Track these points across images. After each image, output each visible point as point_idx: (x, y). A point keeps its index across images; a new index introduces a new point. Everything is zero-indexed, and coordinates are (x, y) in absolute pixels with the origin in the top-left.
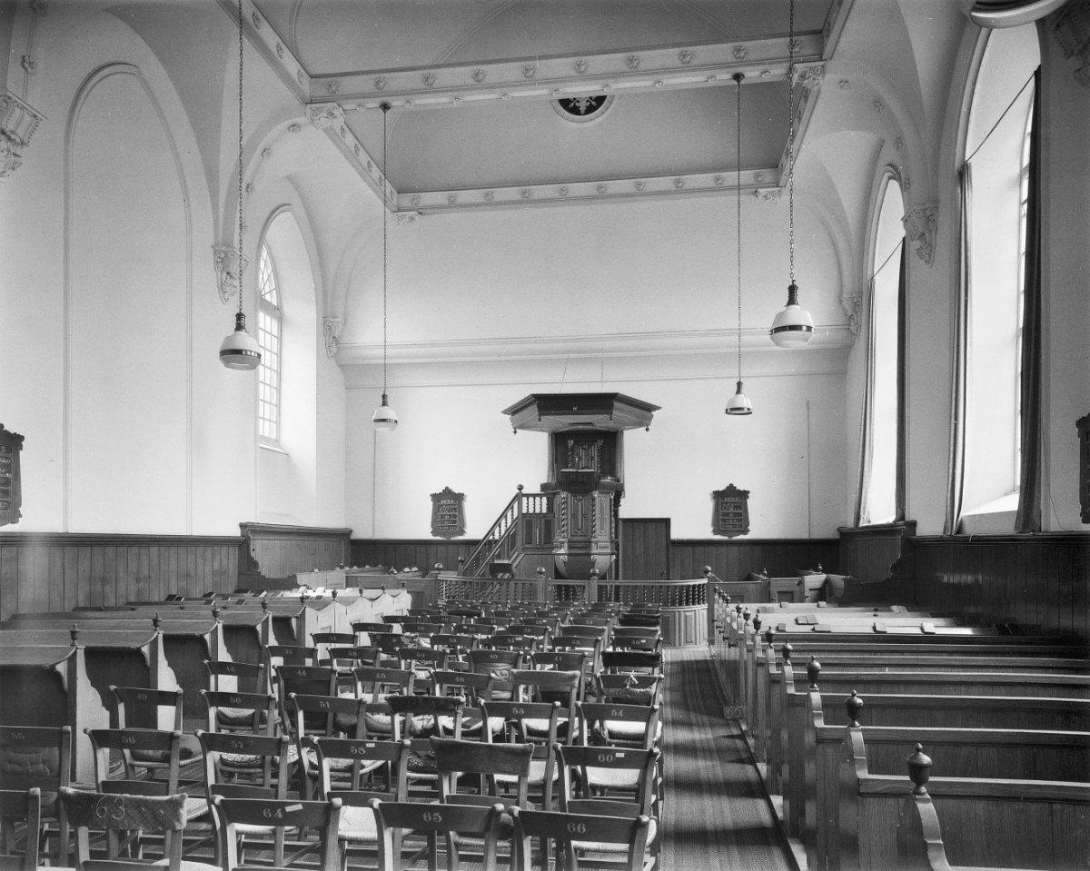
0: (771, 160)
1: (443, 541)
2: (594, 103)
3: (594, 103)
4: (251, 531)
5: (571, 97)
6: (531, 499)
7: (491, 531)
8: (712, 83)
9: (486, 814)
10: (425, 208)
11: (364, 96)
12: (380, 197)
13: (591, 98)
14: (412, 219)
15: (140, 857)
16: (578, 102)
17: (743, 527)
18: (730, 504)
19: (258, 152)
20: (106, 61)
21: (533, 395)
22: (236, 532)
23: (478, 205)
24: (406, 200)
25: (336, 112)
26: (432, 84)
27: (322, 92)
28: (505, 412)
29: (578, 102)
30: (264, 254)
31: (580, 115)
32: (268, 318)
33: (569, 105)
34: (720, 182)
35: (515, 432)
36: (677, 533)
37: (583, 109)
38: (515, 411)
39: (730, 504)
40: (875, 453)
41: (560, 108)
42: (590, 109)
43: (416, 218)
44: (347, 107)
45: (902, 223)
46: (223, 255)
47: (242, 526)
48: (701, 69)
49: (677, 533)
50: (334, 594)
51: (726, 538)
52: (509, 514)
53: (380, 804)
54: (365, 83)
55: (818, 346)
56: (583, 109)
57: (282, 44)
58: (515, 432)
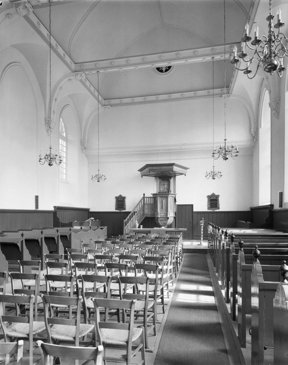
0: (226, 85)
1: (212, 212)
2: (167, 68)
3: (167, 68)
4: (58, 209)
5: (160, 67)
6: (148, 198)
7: (135, 209)
8: (204, 60)
9: (130, 302)
10: (113, 104)
11: (92, 69)
12: (97, 100)
13: (167, 67)
14: (109, 108)
15: (59, 316)
16: (162, 68)
17: (38, 208)
18: (213, 201)
19: (59, 88)
20: (9, 63)
21: (147, 164)
22: (53, 209)
23: (191, 97)
24: (106, 102)
25: (83, 75)
26: (179, 56)
27: (78, 69)
28: (139, 171)
29: (162, 68)
30: (61, 120)
31: (163, 72)
32: (63, 141)
33: (159, 70)
34: (209, 93)
35: (142, 177)
36: (195, 209)
37: (164, 70)
38: (141, 170)
39: (213, 201)
40: (176, 185)
41: (156, 70)
42: (166, 70)
43: (110, 108)
44: (86, 73)
45: (268, 105)
46: (48, 121)
47: (55, 207)
48: (203, 57)
49: (195, 209)
50: (81, 228)
51: (212, 211)
52: (140, 203)
53: (43, 296)
54: (91, 65)
55: (241, 147)
56: (164, 70)
57: (65, 53)
58: (142, 177)
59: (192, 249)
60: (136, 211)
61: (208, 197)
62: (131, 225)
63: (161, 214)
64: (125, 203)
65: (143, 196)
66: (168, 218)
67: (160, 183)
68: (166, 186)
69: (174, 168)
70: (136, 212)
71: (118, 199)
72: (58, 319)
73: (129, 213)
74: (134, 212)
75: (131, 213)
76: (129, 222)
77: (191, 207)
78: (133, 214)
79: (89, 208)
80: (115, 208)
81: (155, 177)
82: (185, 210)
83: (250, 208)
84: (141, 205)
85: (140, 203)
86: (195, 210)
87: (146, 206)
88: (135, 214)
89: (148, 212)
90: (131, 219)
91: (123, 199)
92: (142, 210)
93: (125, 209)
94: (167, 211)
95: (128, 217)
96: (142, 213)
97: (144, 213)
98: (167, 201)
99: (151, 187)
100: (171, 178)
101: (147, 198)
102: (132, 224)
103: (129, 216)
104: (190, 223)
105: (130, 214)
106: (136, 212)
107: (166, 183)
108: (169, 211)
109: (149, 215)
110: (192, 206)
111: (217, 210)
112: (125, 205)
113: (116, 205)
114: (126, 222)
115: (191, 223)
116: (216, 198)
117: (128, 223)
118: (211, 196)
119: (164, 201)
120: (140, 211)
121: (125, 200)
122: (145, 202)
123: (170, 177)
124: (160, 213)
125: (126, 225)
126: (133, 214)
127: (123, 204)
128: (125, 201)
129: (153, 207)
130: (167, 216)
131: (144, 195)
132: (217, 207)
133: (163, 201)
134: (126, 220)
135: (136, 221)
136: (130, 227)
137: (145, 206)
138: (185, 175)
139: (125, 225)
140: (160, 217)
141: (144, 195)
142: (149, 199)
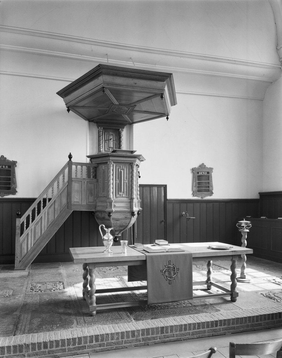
6: (79, 167)
18: (202, 178)
52: (61, 177)
59: (242, 319)
60: (50, 196)
61: (193, 170)
62: (35, 231)
64: (14, 177)
65: (68, 159)
67: (99, 137)
70: (50, 200)
72: (3, 185)
73: (29, 201)
74: (45, 200)
75: (36, 202)
76: (31, 224)
77: (163, 188)
78: (42, 205)
80: (191, 192)
81: (90, 120)
82: (154, 195)
83: (259, 193)
84: (64, 181)
85: (61, 177)
87: (76, 186)
88: (48, 203)
89: (80, 201)
90: (37, 218)
91: (9, 167)
93: (15, 192)
95: (29, 212)
96: (64, 201)
97: (71, 202)
99: (80, 143)
101: (77, 164)
104: (161, 222)
105: (35, 205)
106: (50, 200)
107: (111, 137)
109: (81, 205)
111: (208, 198)
112: (15, 183)
114: (22, 225)
115: (163, 223)
116: (208, 173)
117: (27, 227)
118: (198, 169)
119: (125, 173)
120: (60, 196)
121: (14, 170)
122: (73, 176)
123: (123, 124)
125: (22, 233)
126: (42, 205)
127: (10, 179)
128: (14, 173)
129: (93, 188)
131: (70, 157)
132: (208, 191)
133: (121, 172)
134: (23, 219)
136: (35, 237)
137: (73, 183)
138: (167, 118)
139: (18, 231)
141: (70, 157)
142: (82, 166)
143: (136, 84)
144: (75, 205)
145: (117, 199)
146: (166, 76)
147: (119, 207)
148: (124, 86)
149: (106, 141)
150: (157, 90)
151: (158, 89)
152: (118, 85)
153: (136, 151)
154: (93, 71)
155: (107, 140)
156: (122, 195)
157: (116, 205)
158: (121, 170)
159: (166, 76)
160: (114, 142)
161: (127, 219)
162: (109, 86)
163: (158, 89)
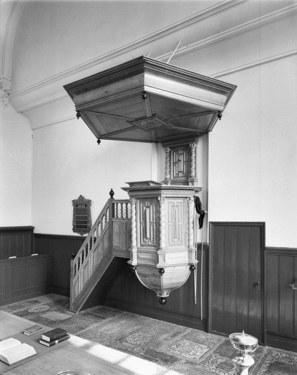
35: (99, 142)
63: (142, 256)
65: (109, 197)
66: (161, 271)
68: (182, 166)
69: (146, 82)
71: (77, 206)
77: (258, 228)
79: (33, 226)
80: (72, 227)
86: (270, 242)
91: (86, 206)
92: (106, 237)
94: (158, 246)
96: (106, 244)
98: (158, 212)
100: (196, 142)
102: (86, 275)
103: (81, 250)
108: (163, 244)
110: (261, 227)
113: (74, 221)
124: (139, 252)
127: (86, 218)
130: (157, 261)
131: (112, 193)
133: (146, 210)
135: (209, 243)
136: (83, 281)
140: (138, 265)
141: (112, 193)
143: (107, 92)
144: (115, 250)
145: (142, 247)
146: (140, 63)
147: (144, 259)
148: (95, 100)
149: (174, 165)
150: (134, 90)
151: (135, 88)
152: (89, 102)
153: (121, 188)
154: (224, 85)
155: (176, 163)
156: (148, 243)
157: (140, 256)
158: (147, 209)
159: (140, 63)
160: (184, 163)
161: (156, 276)
162: (81, 107)
163: (135, 88)
